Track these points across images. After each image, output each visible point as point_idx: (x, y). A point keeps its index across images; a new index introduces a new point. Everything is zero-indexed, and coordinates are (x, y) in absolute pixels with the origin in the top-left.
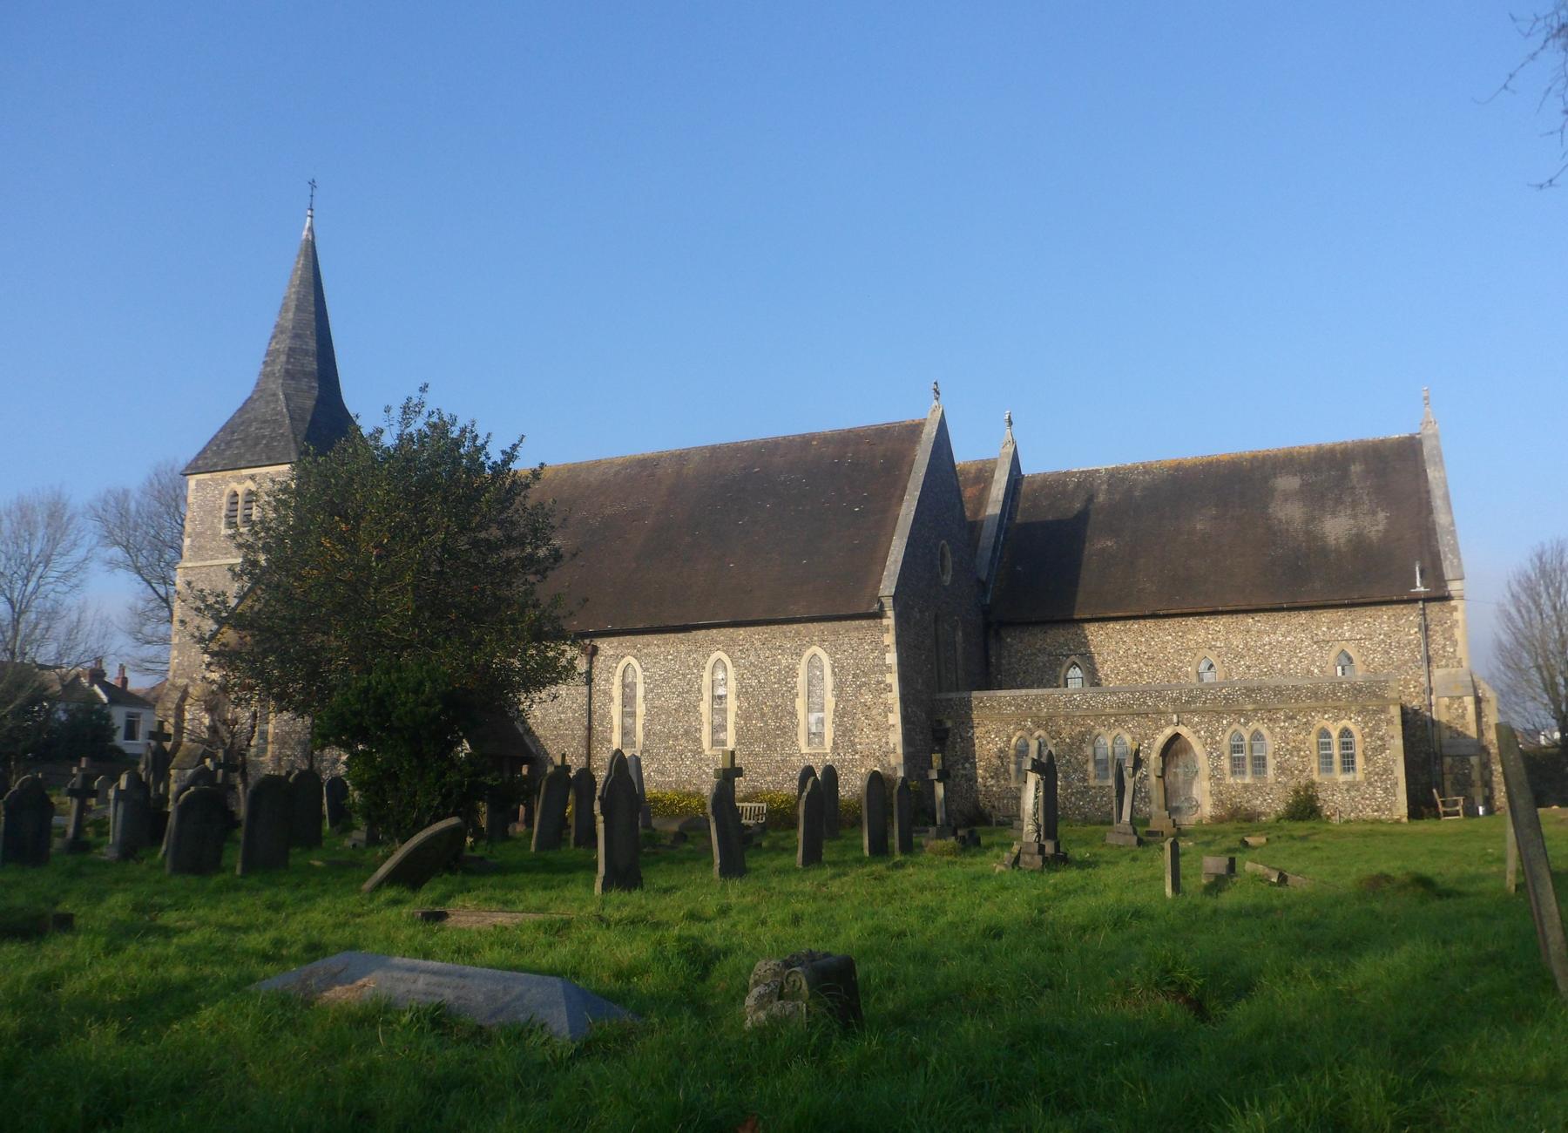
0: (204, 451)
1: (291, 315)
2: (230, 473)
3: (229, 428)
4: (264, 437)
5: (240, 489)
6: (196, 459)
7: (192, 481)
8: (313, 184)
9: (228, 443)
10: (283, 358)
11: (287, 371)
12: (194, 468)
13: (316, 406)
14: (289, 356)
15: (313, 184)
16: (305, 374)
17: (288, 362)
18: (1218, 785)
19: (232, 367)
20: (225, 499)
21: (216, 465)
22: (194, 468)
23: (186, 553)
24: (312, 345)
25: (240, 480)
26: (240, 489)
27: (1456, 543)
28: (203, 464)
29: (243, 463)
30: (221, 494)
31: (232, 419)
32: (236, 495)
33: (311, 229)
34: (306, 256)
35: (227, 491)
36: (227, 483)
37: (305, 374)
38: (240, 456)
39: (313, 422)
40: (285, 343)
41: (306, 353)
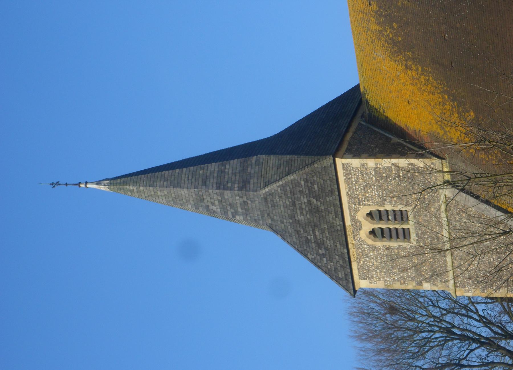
0: (328, 272)
1: (184, 192)
2: (350, 239)
3: (303, 247)
4: (309, 203)
5: (367, 226)
6: (338, 280)
7: (362, 284)
8: (54, 185)
9: (320, 244)
10: (227, 194)
11: (240, 189)
12: (347, 282)
13: (275, 154)
14: (226, 188)
15: (54, 185)
16: (244, 169)
17: (232, 189)
18: (347, 170)
19: (248, 254)
20: (379, 244)
21: (341, 256)
22: (347, 282)
23: (439, 287)
24: (214, 167)
25: (358, 227)
26: (367, 226)
27: (306, 256)
28: (341, 272)
29: (339, 223)
30: (373, 248)
31: (293, 245)
32: (373, 232)
33: (98, 183)
34: (125, 183)
35: (370, 242)
36: (362, 242)
37: (244, 169)
38: (331, 227)
39: (292, 153)
40: (212, 194)
41: (222, 172)
